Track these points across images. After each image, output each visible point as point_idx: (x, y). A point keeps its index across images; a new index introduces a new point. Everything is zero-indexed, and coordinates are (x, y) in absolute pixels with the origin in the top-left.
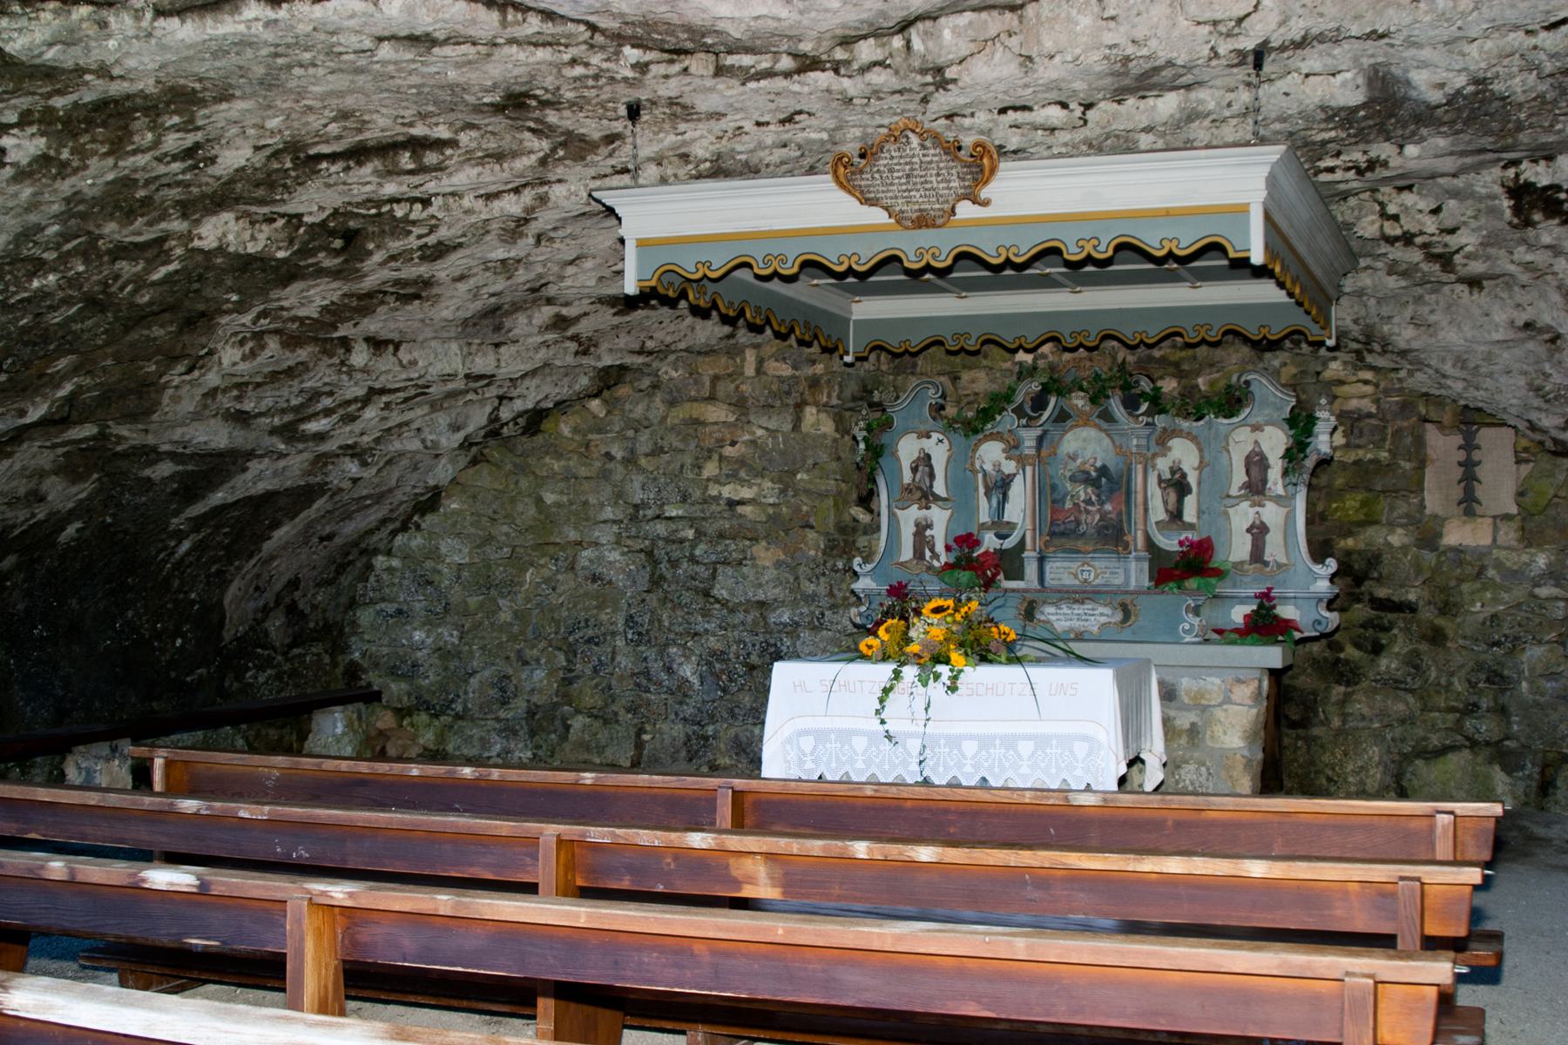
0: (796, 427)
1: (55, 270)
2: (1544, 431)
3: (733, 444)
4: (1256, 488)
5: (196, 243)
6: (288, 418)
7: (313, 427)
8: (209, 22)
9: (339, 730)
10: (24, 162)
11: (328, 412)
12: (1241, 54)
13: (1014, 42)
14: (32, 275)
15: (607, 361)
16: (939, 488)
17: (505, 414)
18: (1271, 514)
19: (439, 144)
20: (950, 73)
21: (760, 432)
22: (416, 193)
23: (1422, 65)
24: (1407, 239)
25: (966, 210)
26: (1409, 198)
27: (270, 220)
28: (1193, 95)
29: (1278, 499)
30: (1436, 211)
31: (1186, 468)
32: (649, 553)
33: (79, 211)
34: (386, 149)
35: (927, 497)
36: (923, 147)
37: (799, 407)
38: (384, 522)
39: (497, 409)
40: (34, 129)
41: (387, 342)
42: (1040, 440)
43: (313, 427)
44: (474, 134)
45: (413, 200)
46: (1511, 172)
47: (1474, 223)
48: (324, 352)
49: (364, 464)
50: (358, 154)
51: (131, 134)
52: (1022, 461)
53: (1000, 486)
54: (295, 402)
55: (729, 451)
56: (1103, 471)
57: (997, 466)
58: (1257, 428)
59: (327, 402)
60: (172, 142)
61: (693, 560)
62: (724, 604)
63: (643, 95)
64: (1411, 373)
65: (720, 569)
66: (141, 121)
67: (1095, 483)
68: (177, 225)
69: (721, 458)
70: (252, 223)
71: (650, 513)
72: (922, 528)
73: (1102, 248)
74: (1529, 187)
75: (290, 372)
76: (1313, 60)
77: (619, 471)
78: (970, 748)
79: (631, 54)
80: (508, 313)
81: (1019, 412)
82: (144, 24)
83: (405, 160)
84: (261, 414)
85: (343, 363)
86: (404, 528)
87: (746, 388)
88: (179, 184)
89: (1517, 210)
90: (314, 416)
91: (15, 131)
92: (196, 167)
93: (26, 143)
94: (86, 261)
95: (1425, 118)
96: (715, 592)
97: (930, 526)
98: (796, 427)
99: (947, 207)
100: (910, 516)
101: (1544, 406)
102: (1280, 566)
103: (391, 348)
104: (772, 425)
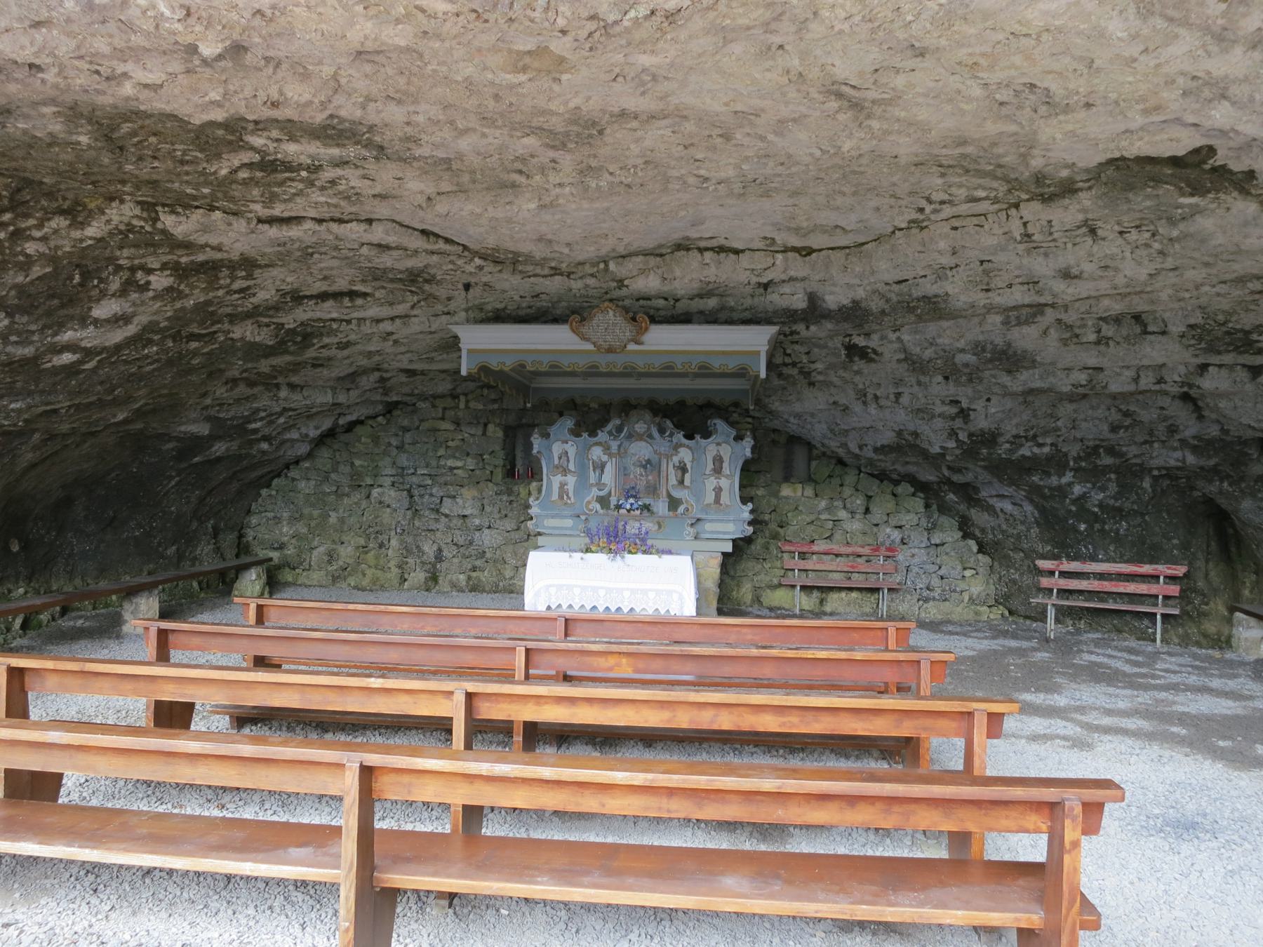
0: (484, 434)
1: (157, 345)
2: (828, 448)
3: (453, 440)
4: (718, 470)
5: (231, 335)
6: (241, 421)
7: (253, 426)
8: (284, 228)
9: (254, 578)
10: (160, 289)
11: (262, 419)
12: (759, 284)
13: (660, 271)
14: (144, 347)
15: (395, 399)
16: (572, 467)
17: (341, 422)
18: (724, 483)
19: (365, 295)
20: (626, 283)
21: (466, 435)
22: (346, 318)
23: (832, 293)
24: (794, 364)
25: (632, 347)
26: (796, 347)
27: (268, 325)
28: (724, 299)
29: (727, 477)
30: (808, 353)
31: (686, 461)
32: (409, 491)
33: (180, 318)
34: (337, 296)
35: (565, 471)
36: (615, 316)
37: (486, 425)
38: (269, 472)
39: (337, 419)
40: (168, 272)
41: (297, 386)
42: (619, 446)
43: (253, 426)
44: (383, 291)
45: (342, 320)
46: (847, 339)
47: (824, 360)
48: (266, 389)
49: (271, 444)
50: (323, 296)
51: (219, 279)
52: (610, 455)
53: (601, 467)
54: (246, 414)
55: (450, 443)
56: (649, 462)
57: (599, 457)
58: (718, 444)
59: (263, 414)
60: (238, 284)
61: (431, 495)
62: (446, 516)
63: (473, 280)
64: (771, 420)
65: (445, 499)
66: (225, 272)
67: (644, 467)
68: (226, 326)
69: (447, 447)
70: (259, 326)
71: (410, 472)
72: (562, 485)
73: (693, 367)
74: (855, 346)
75: (247, 399)
76: (786, 289)
77: (395, 452)
78: (626, 594)
79: (478, 261)
80: (359, 375)
81: (610, 433)
82: (252, 226)
83: (346, 301)
84: (228, 419)
85: (275, 396)
86: (279, 475)
87: (460, 414)
88: (232, 305)
89: (848, 356)
90: (255, 421)
91: (158, 273)
92: (244, 298)
93: (163, 280)
94: (174, 341)
95: (827, 315)
96: (442, 510)
97: (566, 484)
98: (484, 434)
99: (623, 344)
100: (557, 480)
101: (833, 437)
102: (727, 506)
103: (299, 389)
104: (472, 432)
